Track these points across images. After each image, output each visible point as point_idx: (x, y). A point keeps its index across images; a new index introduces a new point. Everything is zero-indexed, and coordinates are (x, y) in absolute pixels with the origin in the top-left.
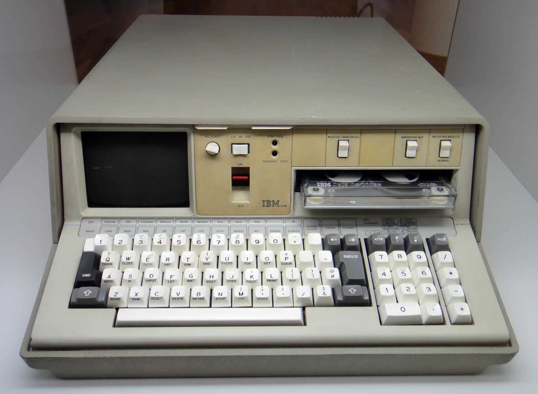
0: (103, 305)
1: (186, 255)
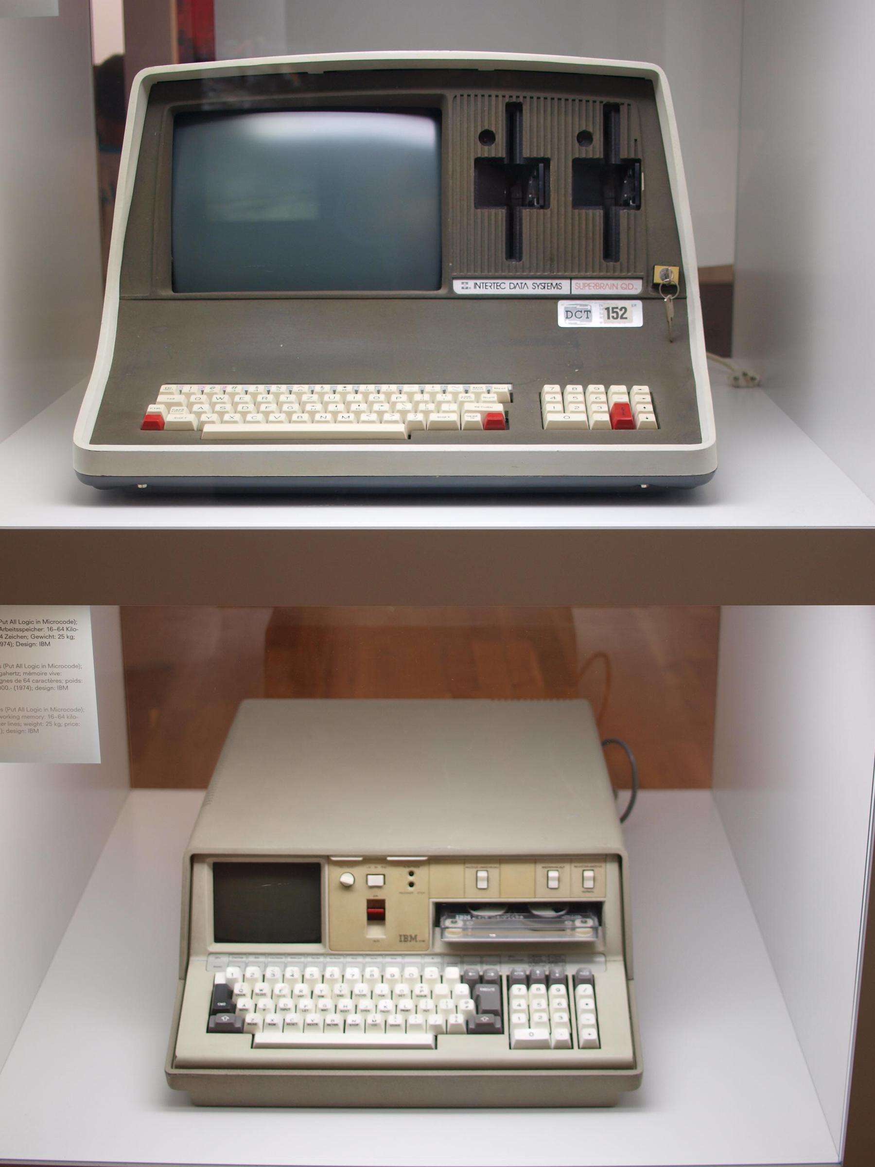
0: (239, 1031)
1: (319, 988)
